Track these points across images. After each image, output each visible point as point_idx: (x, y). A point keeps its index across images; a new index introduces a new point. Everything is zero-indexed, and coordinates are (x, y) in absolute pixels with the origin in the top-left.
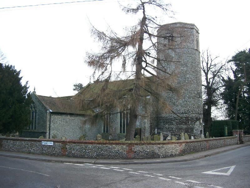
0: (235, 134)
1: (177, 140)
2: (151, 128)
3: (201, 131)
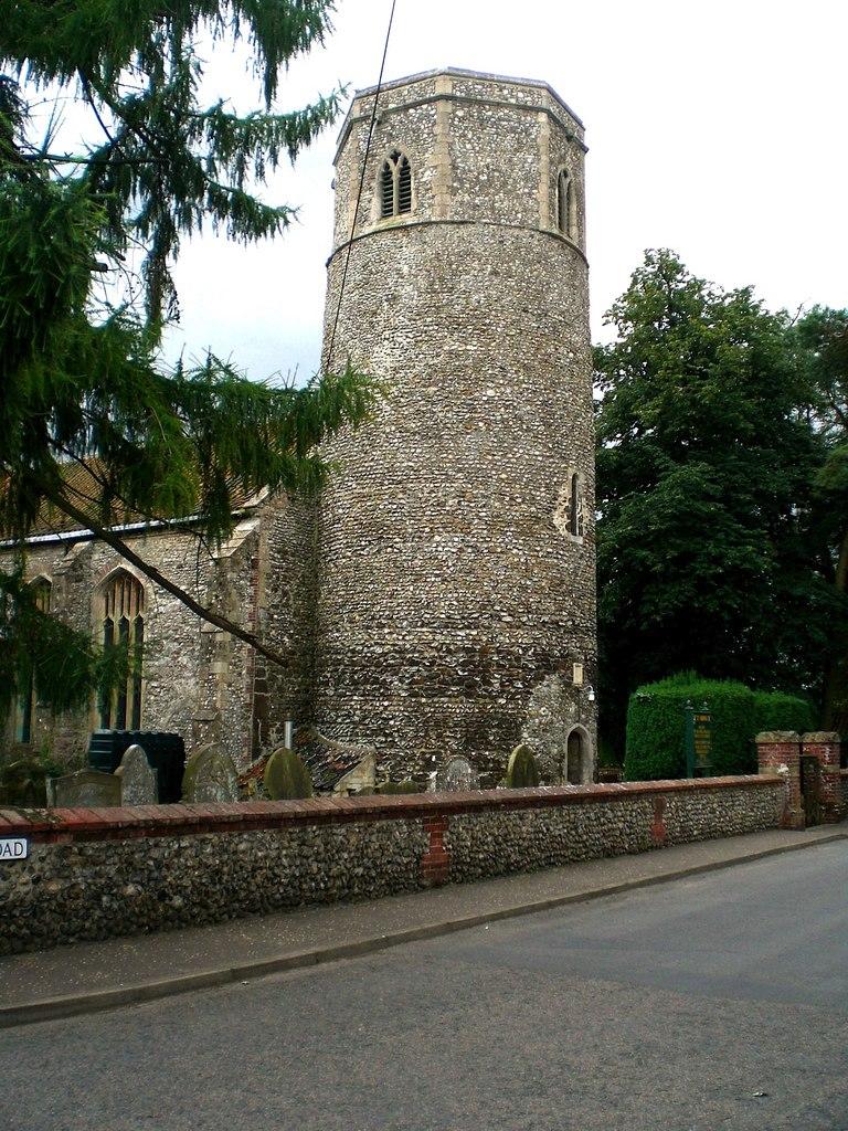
0: (771, 756)
1: (484, 783)
2: (258, 714)
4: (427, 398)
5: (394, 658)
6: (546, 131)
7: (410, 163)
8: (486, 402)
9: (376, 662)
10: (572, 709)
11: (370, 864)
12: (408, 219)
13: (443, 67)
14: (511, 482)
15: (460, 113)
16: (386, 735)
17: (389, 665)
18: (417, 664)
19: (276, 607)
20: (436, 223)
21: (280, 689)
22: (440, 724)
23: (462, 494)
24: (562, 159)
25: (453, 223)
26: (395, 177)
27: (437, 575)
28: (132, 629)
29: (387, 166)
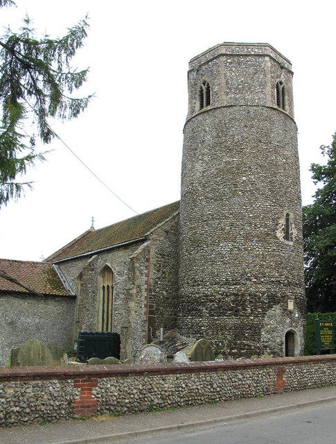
2: (149, 325)
3: (290, 335)
4: (216, 183)
5: (203, 299)
6: (269, 64)
7: (210, 85)
8: (242, 183)
9: (196, 301)
10: (288, 321)
11: (25, 405)
12: (209, 108)
13: (221, 42)
14: (254, 218)
15: (229, 61)
16: (200, 334)
17: (202, 302)
18: (213, 301)
19: (159, 278)
20: (220, 108)
21: (162, 314)
22: (223, 328)
23: (232, 225)
24: (279, 76)
25: (226, 107)
26: (205, 91)
27: (221, 261)
28: (106, 289)
29: (201, 88)
